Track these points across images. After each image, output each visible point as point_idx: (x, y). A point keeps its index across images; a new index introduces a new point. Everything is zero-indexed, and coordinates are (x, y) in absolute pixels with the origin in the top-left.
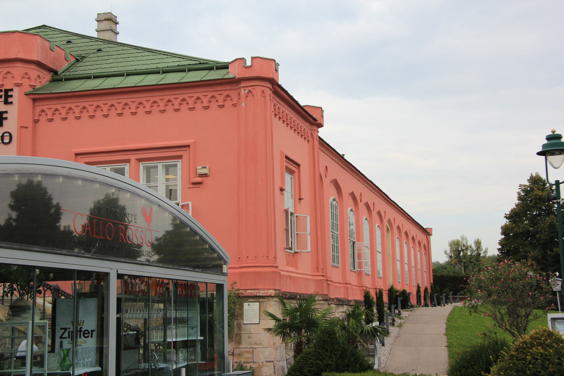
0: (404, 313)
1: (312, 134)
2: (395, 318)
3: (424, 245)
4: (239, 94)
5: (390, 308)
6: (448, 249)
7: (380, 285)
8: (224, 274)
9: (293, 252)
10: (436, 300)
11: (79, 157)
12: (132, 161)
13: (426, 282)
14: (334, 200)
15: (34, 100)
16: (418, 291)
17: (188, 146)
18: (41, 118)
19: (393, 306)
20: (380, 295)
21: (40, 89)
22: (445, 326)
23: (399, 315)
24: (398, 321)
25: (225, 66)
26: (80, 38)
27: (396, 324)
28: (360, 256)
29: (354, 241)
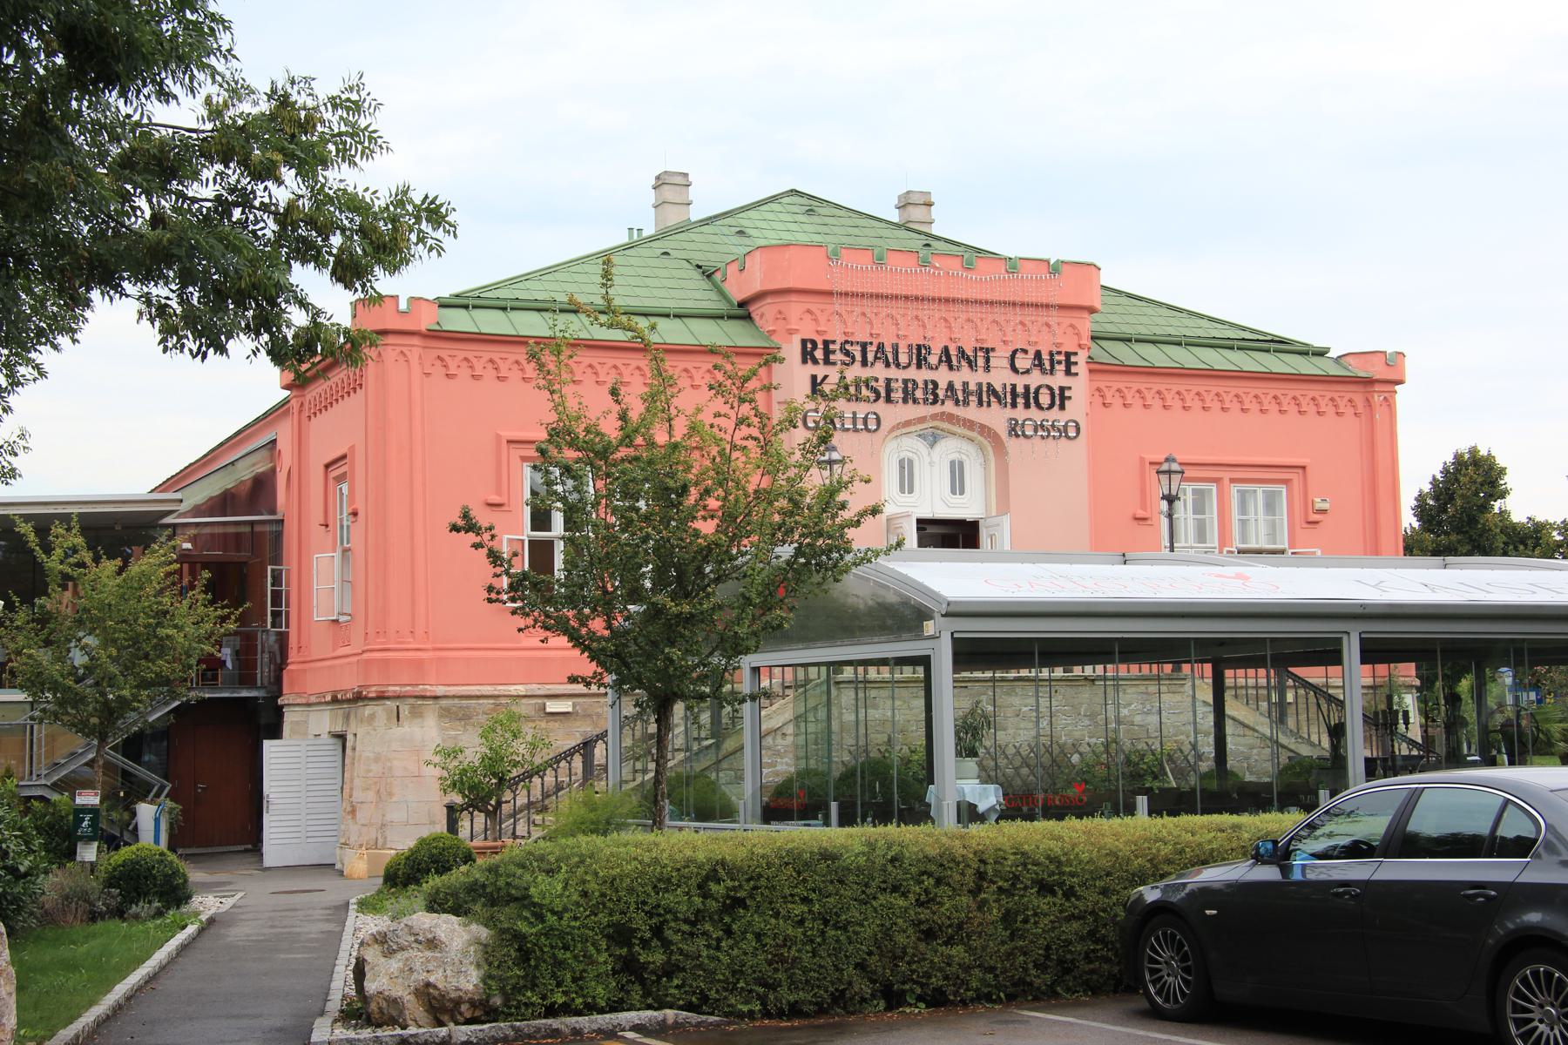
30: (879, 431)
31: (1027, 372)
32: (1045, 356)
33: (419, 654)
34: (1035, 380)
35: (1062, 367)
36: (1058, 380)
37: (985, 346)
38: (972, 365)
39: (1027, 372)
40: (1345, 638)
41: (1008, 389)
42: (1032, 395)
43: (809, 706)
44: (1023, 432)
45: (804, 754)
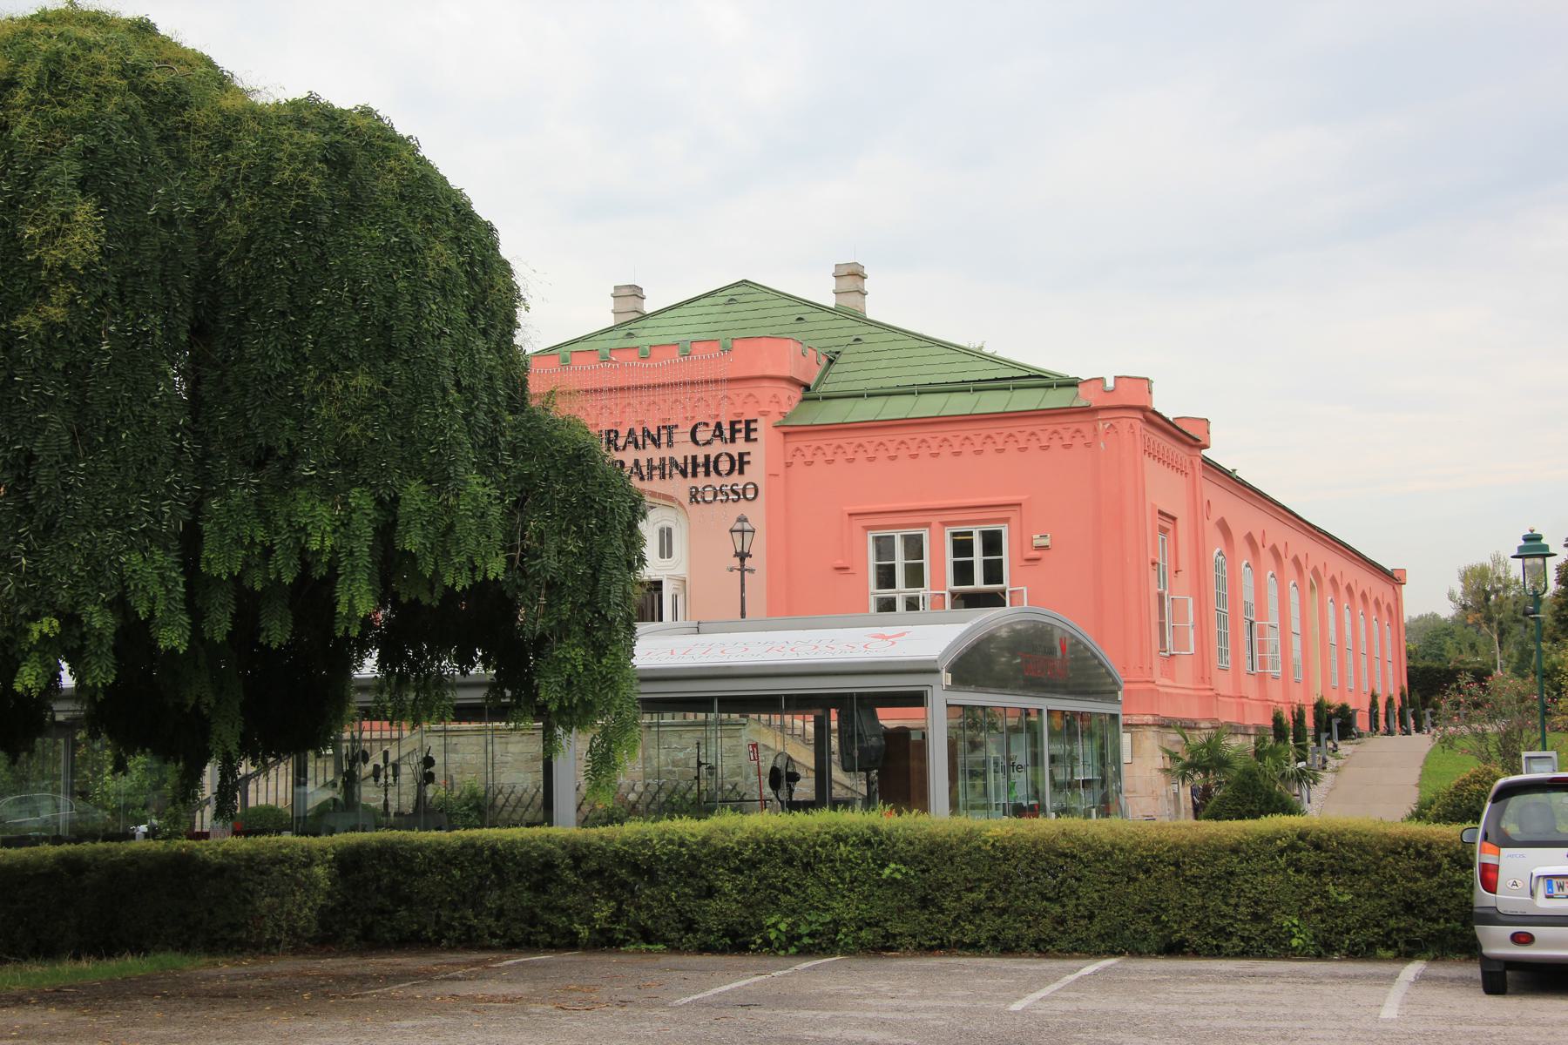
0: (1345, 748)
1: (1191, 462)
2: (1328, 757)
3: (1389, 606)
4: (1095, 429)
5: (1317, 739)
6: (1458, 589)
7: (1298, 697)
8: (1119, 702)
9: (1167, 654)
10: (1412, 721)
11: (854, 518)
12: (933, 526)
13: (1391, 683)
14: (1220, 554)
15: (785, 434)
16: (1374, 704)
17: (1020, 505)
19: (1324, 736)
20: (1299, 720)
22: (1419, 771)
23: (1334, 751)
24: (1332, 762)
25: (1072, 384)
26: (814, 310)
27: (1329, 768)
28: (1262, 645)
29: (1252, 619)
30: (711, 505)
31: (708, 443)
32: (726, 427)
34: (717, 448)
35: (743, 435)
36: (740, 446)
37: (667, 424)
38: (656, 442)
39: (708, 443)
40: (929, 689)
41: (689, 461)
42: (712, 464)
43: (402, 754)
44: (703, 498)
45: (402, 797)
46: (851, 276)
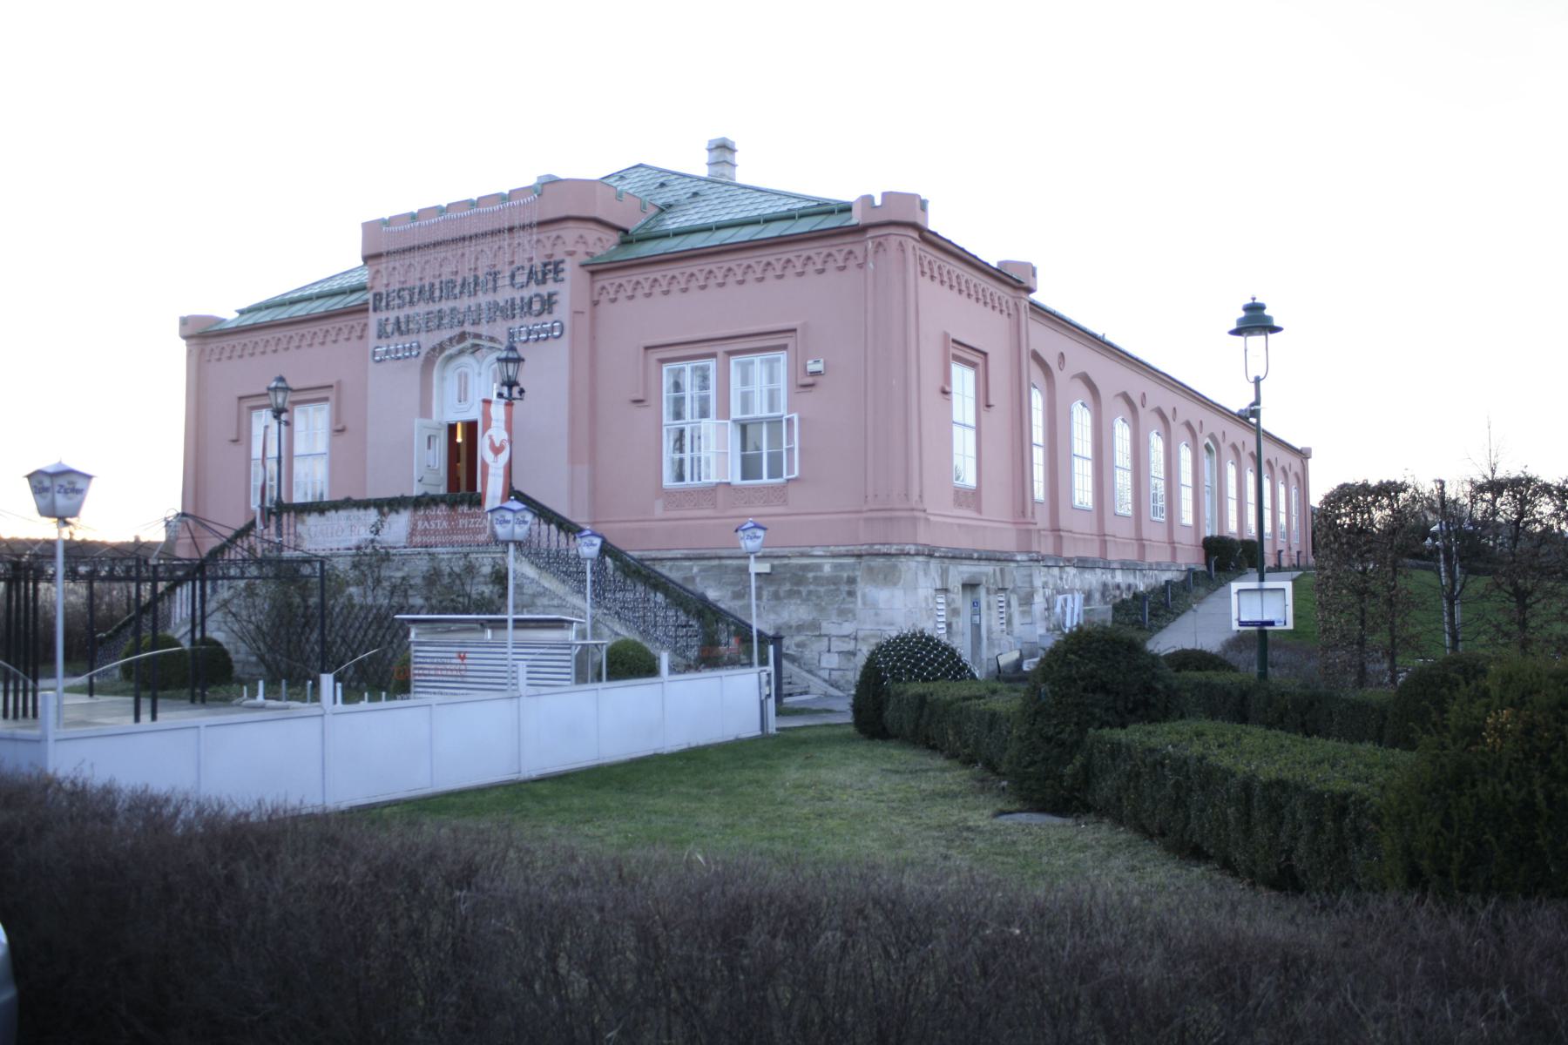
1: (1016, 304)
11: (650, 351)
15: (593, 273)
17: (794, 330)
18: (602, 298)
21: (598, 258)
25: (846, 209)
33: (628, 525)
46: (723, 149)
